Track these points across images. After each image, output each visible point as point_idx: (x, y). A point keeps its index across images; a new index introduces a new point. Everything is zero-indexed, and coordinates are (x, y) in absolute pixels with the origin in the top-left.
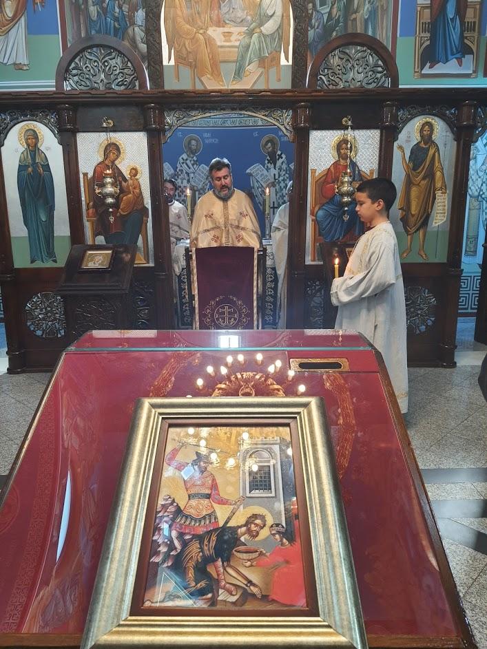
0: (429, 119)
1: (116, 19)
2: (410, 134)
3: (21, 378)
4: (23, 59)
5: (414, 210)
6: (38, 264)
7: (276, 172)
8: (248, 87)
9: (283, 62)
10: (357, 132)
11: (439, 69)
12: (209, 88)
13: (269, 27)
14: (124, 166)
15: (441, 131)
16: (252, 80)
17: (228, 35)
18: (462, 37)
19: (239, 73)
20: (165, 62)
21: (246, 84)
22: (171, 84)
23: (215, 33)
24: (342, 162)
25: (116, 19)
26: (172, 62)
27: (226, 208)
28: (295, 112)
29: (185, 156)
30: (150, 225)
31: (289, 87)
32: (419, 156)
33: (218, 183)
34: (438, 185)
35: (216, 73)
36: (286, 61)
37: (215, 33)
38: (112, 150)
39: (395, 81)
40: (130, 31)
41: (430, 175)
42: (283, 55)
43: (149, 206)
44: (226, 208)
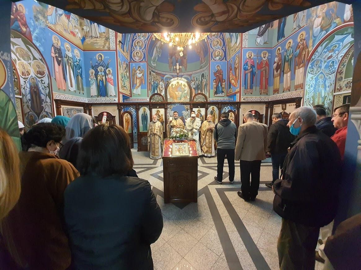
0: (213, 106)
1: (156, 84)
2: (210, 109)
3: (140, 152)
4: (140, 93)
5: (11, 170)
6: (144, 131)
7: (188, 112)
8: (182, 101)
9: (188, 97)
10: (201, 109)
11: (218, 95)
12: (176, 101)
13: (185, 92)
14: (160, 114)
15: (215, 108)
16: (183, 100)
17: (179, 93)
18: (222, 90)
19: (180, 99)
20: (168, 97)
21: (182, 101)
22: (169, 101)
23: (177, 93)
24: (199, 113)
25: (156, 84)
26: (169, 97)
27: (176, 122)
28: (190, 105)
29: (169, 109)
30: (164, 124)
31: (189, 101)
32: (212, 113)
33: (175, 115)
34: (216, 117)
35: (176, 99)
36: (189, 97)
37: (177, 93)
38: (158, 111)
39: (207, 100)
40: (159, 86)
41: (214, 116)
42: (188, 96)
43: (164, 121)
44: (176, 122)
